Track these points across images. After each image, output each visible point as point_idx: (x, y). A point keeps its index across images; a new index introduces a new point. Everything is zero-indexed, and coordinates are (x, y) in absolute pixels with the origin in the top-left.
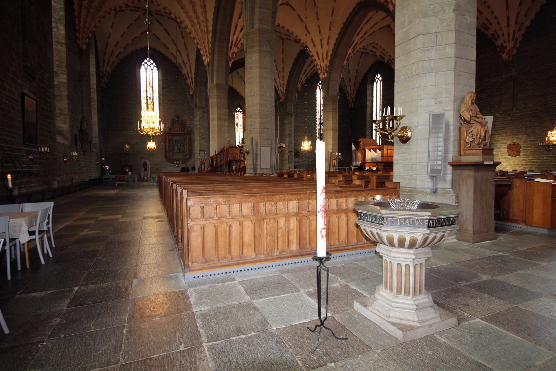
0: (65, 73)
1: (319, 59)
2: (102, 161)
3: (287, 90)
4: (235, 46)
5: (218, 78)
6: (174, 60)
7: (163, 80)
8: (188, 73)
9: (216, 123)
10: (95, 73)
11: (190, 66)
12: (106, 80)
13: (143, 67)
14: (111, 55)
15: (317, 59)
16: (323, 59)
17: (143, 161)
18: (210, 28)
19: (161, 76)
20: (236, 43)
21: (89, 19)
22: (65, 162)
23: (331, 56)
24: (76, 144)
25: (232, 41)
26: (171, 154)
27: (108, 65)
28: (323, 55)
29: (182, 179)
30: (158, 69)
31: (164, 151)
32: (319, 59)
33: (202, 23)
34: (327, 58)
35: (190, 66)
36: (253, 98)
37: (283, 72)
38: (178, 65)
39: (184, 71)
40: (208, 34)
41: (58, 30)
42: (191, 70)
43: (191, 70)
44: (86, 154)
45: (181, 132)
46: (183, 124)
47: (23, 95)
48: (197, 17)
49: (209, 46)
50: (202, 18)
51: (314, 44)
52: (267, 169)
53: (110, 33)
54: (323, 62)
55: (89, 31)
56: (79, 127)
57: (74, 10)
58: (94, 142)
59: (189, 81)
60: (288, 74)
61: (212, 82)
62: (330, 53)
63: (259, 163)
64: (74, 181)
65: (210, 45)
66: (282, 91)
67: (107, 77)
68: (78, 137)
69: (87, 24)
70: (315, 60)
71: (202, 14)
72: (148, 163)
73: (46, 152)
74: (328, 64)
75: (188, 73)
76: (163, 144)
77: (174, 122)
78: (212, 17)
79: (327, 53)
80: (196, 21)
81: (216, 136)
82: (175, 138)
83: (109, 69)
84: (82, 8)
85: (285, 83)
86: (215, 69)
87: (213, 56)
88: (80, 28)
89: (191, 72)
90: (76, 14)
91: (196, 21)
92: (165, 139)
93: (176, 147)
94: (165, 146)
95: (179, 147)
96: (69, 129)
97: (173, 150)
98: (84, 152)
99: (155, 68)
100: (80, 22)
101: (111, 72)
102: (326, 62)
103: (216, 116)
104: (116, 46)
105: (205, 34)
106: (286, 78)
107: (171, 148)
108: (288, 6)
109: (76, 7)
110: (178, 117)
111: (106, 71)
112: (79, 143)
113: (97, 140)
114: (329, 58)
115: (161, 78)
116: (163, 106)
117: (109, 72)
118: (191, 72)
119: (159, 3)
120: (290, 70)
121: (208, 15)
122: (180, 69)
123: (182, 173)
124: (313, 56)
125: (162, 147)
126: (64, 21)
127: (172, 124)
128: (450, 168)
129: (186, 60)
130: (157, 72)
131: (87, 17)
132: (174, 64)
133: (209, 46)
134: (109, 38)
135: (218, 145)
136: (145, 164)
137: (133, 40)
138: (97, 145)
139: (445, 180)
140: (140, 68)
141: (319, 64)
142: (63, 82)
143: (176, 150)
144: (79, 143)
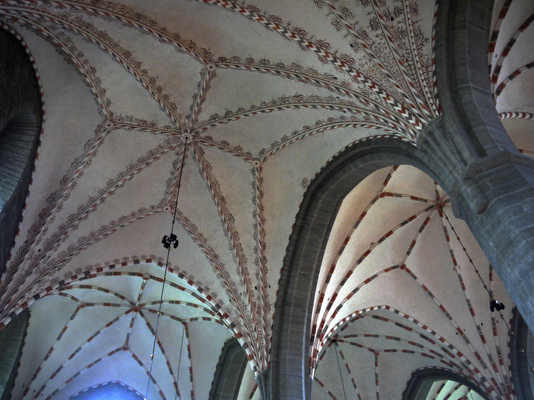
1: (485, 367)
4: (318, 336)
5: (494, 87)
15: (480, 368)
16: (494, 366)
18: (273, 299)
20: (320, 330)
21: (29, 280)
23: (510, 356)
25: (315, 326)
28: (490, 357)
32: (485, 367)
34: (501, 362)
48: (247, 282)
54: (496, 370)
55: (20, 302)
57: (9, 256)
62: (506, 351)
65: (270, 333)
74: (510, 374)
78: (278, 276)
79: (499, 353)
80: (242, 289)
84: (27, 256)
90: (8, 264)
102: (504, 370)
108: (404, 271)
109: (14, 252)
114: (507, 361)
121: (268, 275)
123: (502, 377)
131: (28, 273)
134: (46, 358)
141: (488, 377)
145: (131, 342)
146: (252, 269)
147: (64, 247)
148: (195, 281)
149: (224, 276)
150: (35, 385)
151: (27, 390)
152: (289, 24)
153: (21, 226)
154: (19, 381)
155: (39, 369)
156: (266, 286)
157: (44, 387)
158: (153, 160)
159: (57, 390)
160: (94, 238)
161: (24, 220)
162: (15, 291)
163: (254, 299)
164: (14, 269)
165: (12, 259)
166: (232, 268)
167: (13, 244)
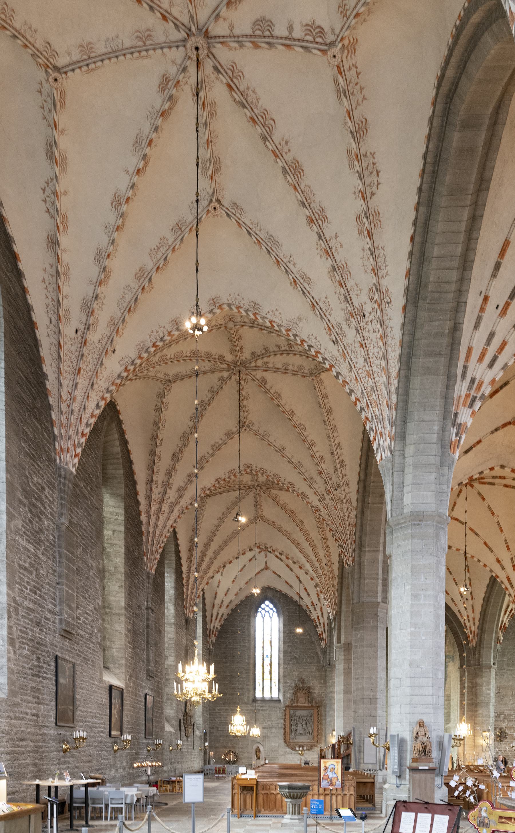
0: (173, 654)
2: (205, 746)
3: (481, 628)
6: (301, 602)
7: (284, 632)
8: (318, 617)
9: (342, 697)
10: (201, 635)
11: (321, 608)
12: (213, 638)
13: (259, 614)
14: (220, 607)
17: (254, 747)
19: (282, 625)
22: (170, 751)
24: (180, 730)
26: (292, 736)
27: (216, 618)
29: (311, 773)
30: (279, 616)
31: (283, 731)
33: (326, 568)
35: (321, 608)
36: (358, 681)
37: (472, 599)
38: (305, 608)
39: (314, 616)
40: (333, 580)
41: (169, 610)
42: (322, 614)
43: (322, 614)
44: (189, 739)
45: (307, 705)
46: (308, 691)
47: (146, 695)
49: (335, 595)
50: (324, 562)
51: (501, 565)
52: (372, 764)
53: (219, 581)
56: (184, 709)
57: (182, 578)
58: (198, 722)
59: (320, 629)
60: (481, 602)
61: (339, 641)
63: (362, 757)
64: (177, 771)
66: (473, 629)
67: (215, 635)
68: (182, 721)
69: (195, 591)
70: (507, 589)
71: (325, 557)
72: (261, 749)
73: (160, 744)
75: (318, 617)
76: (282, 721)
77: (297, 690)
80: (318, 565)
81: (342, 714)
82: (299, 713)
83: (218, 625)
85: (478, 616)
86: (343, 624)
87: (340, 608)
88: (187, 597)
89: (322, 616)
90: (184, 582)
91: (318, 565)
92: (285, 715)
93: (300, 725)
94: (285, 725)
95: (304, 726)
96: (174, 715)
97: (296, 730)
98: (187, 737)
99: (275, 615)
100: (188, 590)
101: (219, 628)
103: (342, 688)
104: (226, 595)
105: (329, 580)
106: (478, 609)
107: (294, 727)
109: (184, 575)
110: (303, 683)
111: (214, 626)
112: (183, 728)
113: (201, 719)
115: (282, 629)
116: (284, 668)
117: (217, 628)
118: (322, 616)
119: (274, 549)
120: (483, 595)
122: (308, 613)
124: (502, 582)
125: (280, 725)
126: (173, 600)
127: (295, 693)
128: (408, 770)
129: (316, 601)
130: (277, 619)
132: (300, 607)
133: (335, 595)
134: (218, 586)
135: (345, 727)
136: (258, 751)
137: (247, 583)
138: (201, 726)
139: (405, 779)
140: (255, 617)
142: (171, 665)
143: (300, 729)
144: (183, 728)
145: (268, 565)
146: (322, 553)
147: (207, 560)
148: (290, 557)
149: (306, 557)
150: (218, 602)
151: (214, 606)
152: (285, 479)
153: (182, 562)
154: (207, 601)
155: (216, 593)
156: (332, 563)
157: (223, 601)
158: (224, 81)
159: (231, 601)
160: (221, 549)
161: (183, 565)
162: (192, 593)
163: (325, 572)
164: (188, 584)
165: (185, 578)
166: (309, 551)
167: (182, 572)
